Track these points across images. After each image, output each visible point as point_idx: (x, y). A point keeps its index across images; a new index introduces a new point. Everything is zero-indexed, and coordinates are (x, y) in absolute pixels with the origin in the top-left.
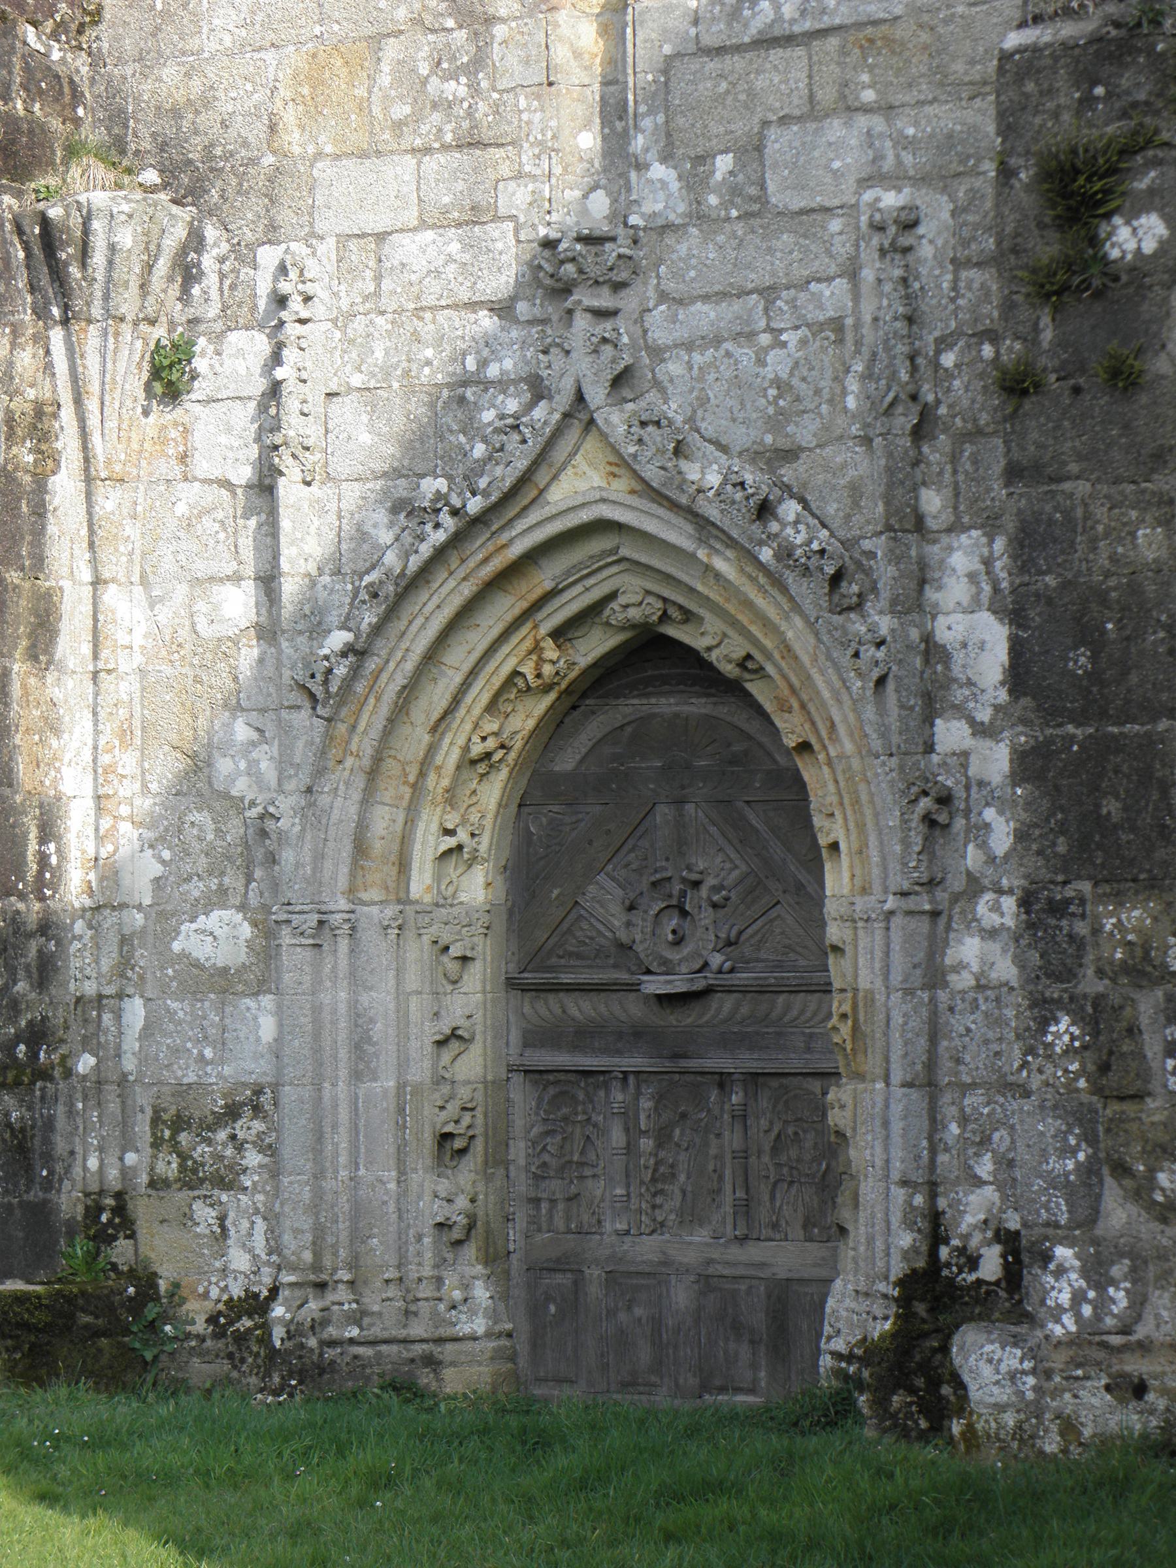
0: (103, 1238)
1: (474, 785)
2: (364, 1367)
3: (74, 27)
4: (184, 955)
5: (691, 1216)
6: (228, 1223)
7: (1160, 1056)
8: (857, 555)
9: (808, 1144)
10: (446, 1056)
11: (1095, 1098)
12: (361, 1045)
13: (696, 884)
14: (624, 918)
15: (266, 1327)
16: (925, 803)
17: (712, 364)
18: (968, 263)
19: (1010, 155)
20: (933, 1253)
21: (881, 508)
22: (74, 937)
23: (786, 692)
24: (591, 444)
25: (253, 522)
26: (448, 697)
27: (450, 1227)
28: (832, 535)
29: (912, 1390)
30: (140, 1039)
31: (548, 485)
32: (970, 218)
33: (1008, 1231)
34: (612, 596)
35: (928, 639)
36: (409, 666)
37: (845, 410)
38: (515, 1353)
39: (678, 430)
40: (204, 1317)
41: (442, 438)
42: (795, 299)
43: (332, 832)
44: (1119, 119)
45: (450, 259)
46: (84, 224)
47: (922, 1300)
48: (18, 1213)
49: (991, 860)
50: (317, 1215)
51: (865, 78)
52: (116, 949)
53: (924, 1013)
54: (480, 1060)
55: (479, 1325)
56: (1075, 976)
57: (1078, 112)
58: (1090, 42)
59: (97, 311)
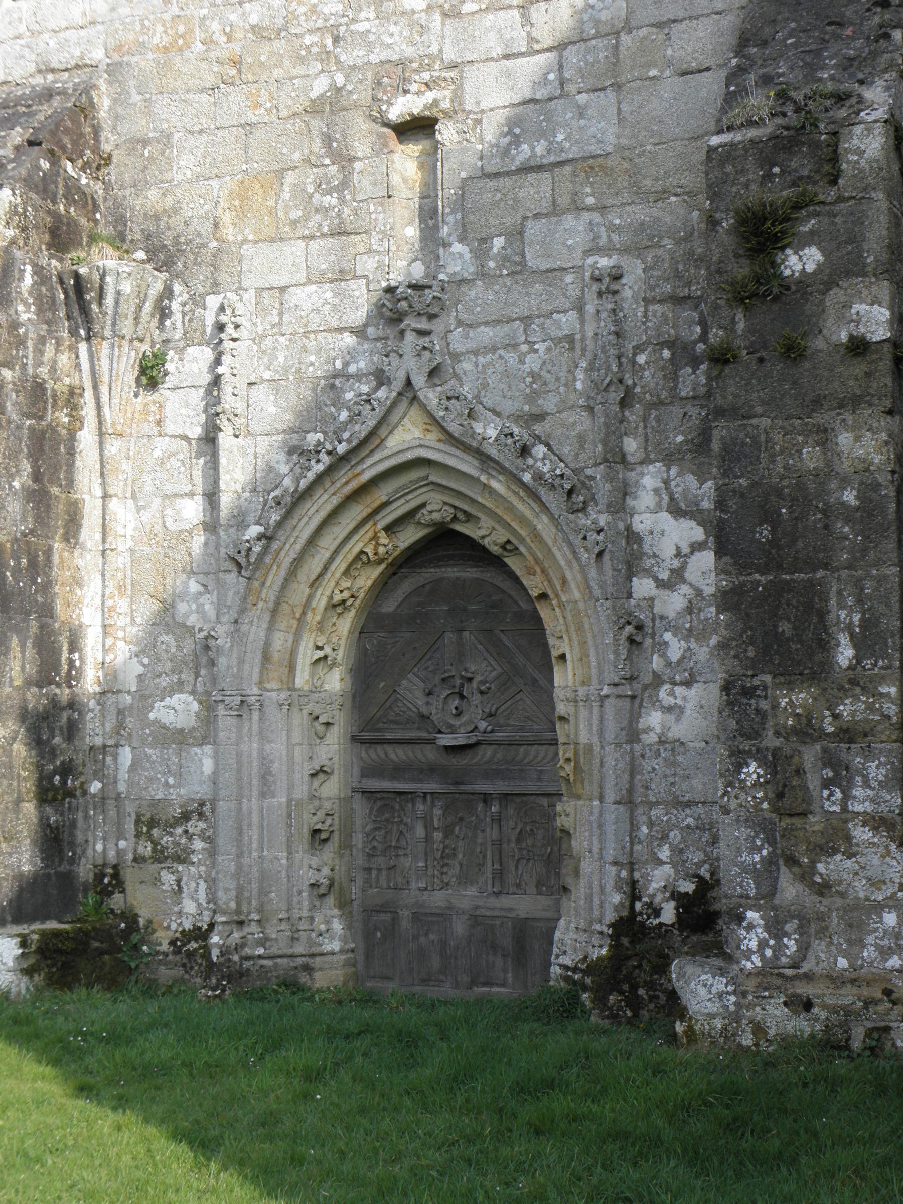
0: (106, 893)
1: (334, 620)
2: (267, 972)
3: (94, 165)
4: (156, 722)
5: (465, 880)
6: (183, 884)
7: (818, 788)
8: (582, 478)
9: (539, 837)
10: (316, 783)
11: (774, 815)
12: (266, 775)
13: (470, 680)
14: (425, 699)
15: (207, 949)
16: (629, 629)
17: (490, 363)
18: (654, 301)
19: (716, 211)
20: (632, 907)
21: (600, 448)
22: (89, 710)
23: (533, 563)
24: (414, 412)
25: (202, 461)
26: (321, 566)
27: (318, 886)
28: (567, 466)
29: (621, 993)
30: (129, 772)
31: (387, 437)
32: (655, 273)
33: (679, 893)
34: (423, 505)
35: (628, 528)
36: (298, 547)
37: (575, 390)
38: (356, 961)
39: (471, 403)
40: (167, 941)
41: (320, 409)
42: (543, 324)
43: (249, 648)
44: (790, 187)
45: (326, 302)
46: (101, 279)
47: (626, 936)
48: (54, 878)
49: (669, 664)
50: (238, 880)
51: (588, 190)
52: (115, 717)
53: (628, 759)
54: (337, 785)
55: (336, 946)
56: (760, 736)
57: (761, 183)
58: (769, 139)
59: (108, 333)
